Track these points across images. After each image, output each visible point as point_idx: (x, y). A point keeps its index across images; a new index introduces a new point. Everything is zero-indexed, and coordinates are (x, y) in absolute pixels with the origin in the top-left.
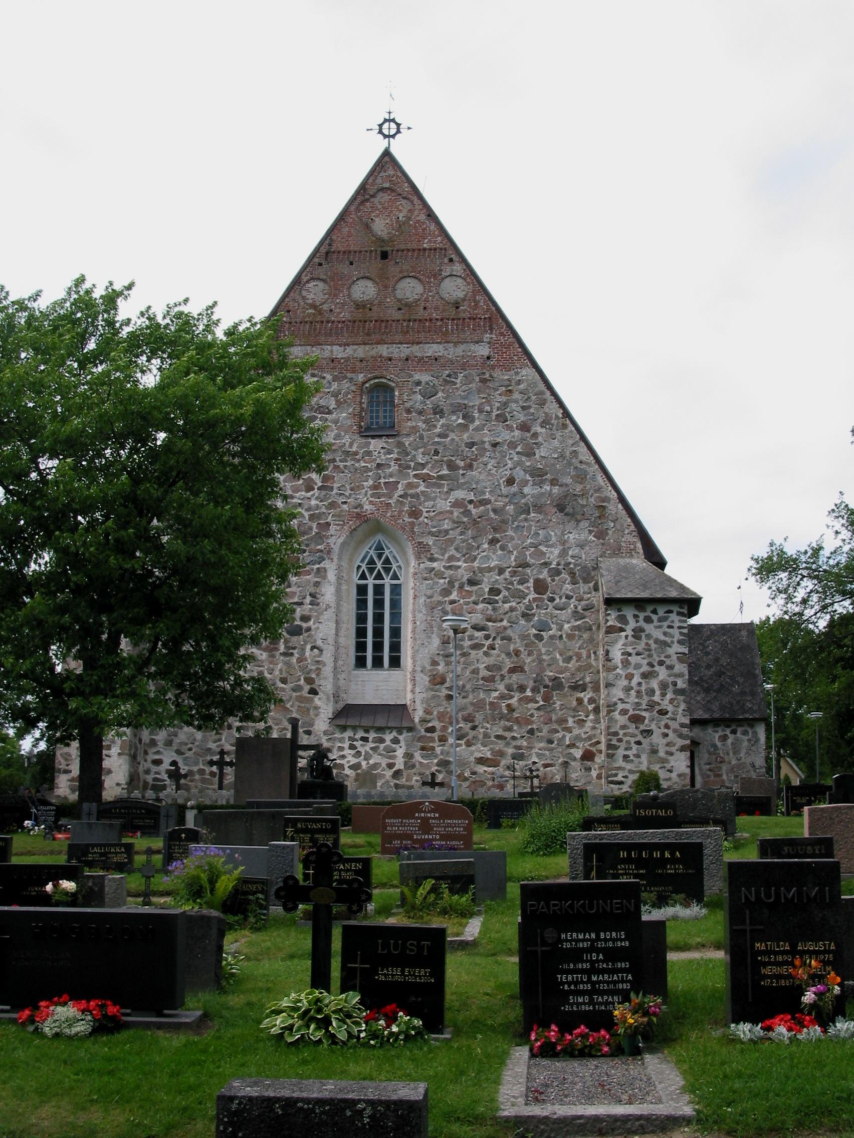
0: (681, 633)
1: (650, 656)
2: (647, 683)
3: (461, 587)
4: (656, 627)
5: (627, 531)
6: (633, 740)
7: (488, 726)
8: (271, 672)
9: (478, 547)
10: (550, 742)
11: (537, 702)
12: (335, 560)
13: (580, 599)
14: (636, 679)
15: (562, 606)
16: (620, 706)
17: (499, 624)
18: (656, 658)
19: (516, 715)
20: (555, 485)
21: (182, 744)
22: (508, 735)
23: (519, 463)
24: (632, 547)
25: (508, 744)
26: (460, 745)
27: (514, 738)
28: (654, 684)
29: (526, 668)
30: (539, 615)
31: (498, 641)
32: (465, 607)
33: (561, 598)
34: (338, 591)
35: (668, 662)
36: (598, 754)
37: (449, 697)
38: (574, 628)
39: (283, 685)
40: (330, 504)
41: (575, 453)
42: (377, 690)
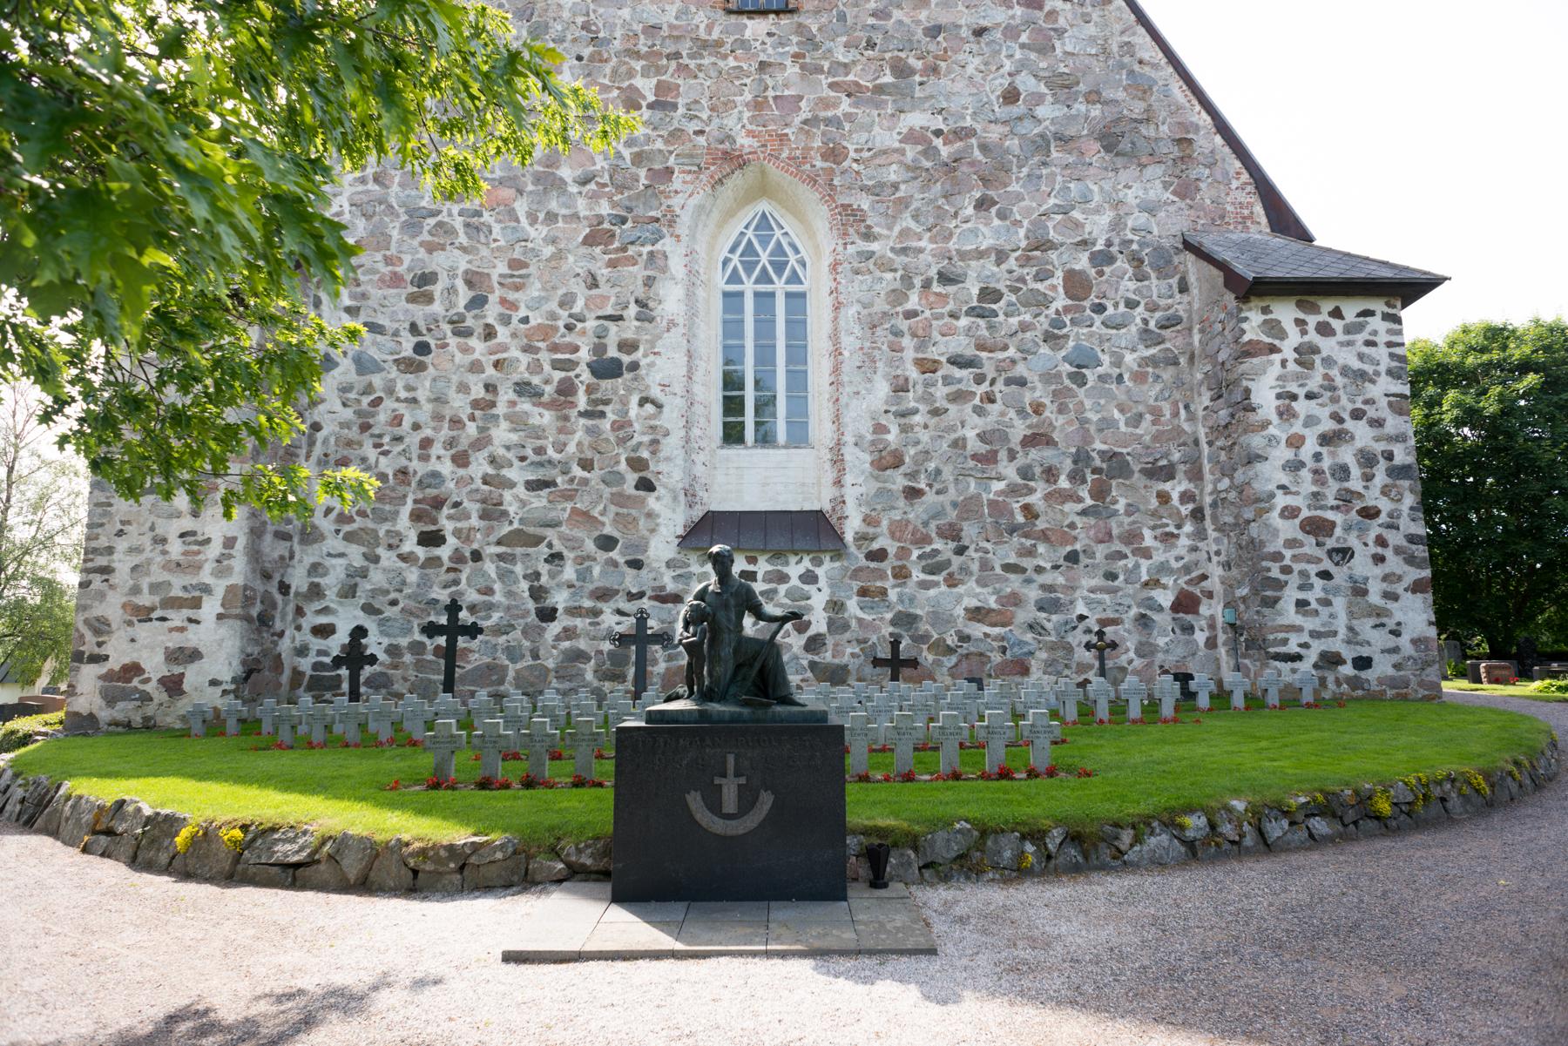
0: (1392, 356)
1: (1335, 400)
2: (1333, 454)
3: (927, 285)
4: (1341, 344)
5: (1235, 184)
6: (1313, 569)
7: (988, 546)
8: (560, 447)
9: (956, 215)
10: (1112, 576)
11: (1080, 500)
12: (684, 238)
13: (1153, 308)
14: (1310, 446)
15: (1119, 320)
16: (1281, 500)
17: (1000, 355)
18: (1346, 405)
19: (1041, 524)
20: (1094, 103)
21: (376, 592)
22: (1028, 563)
23: (1022, 66)
24: (1246, 212)
25: (1029, 581)
26: (936, 584)
27: (1039, 570)
28: (1347, 455)
29: (1056, 436)
30: (1076, 336)
31: (999, 385)
32: (935, 323)
33: (1116, 305)
34: (690, 295)
35: (1371, 413)
36: (1205, 600)
37: (913, 493)
38: (1145, 362)
39: (585, 474)
40: (671, 134)
41: (1128, 47)
42: (765, 485)
